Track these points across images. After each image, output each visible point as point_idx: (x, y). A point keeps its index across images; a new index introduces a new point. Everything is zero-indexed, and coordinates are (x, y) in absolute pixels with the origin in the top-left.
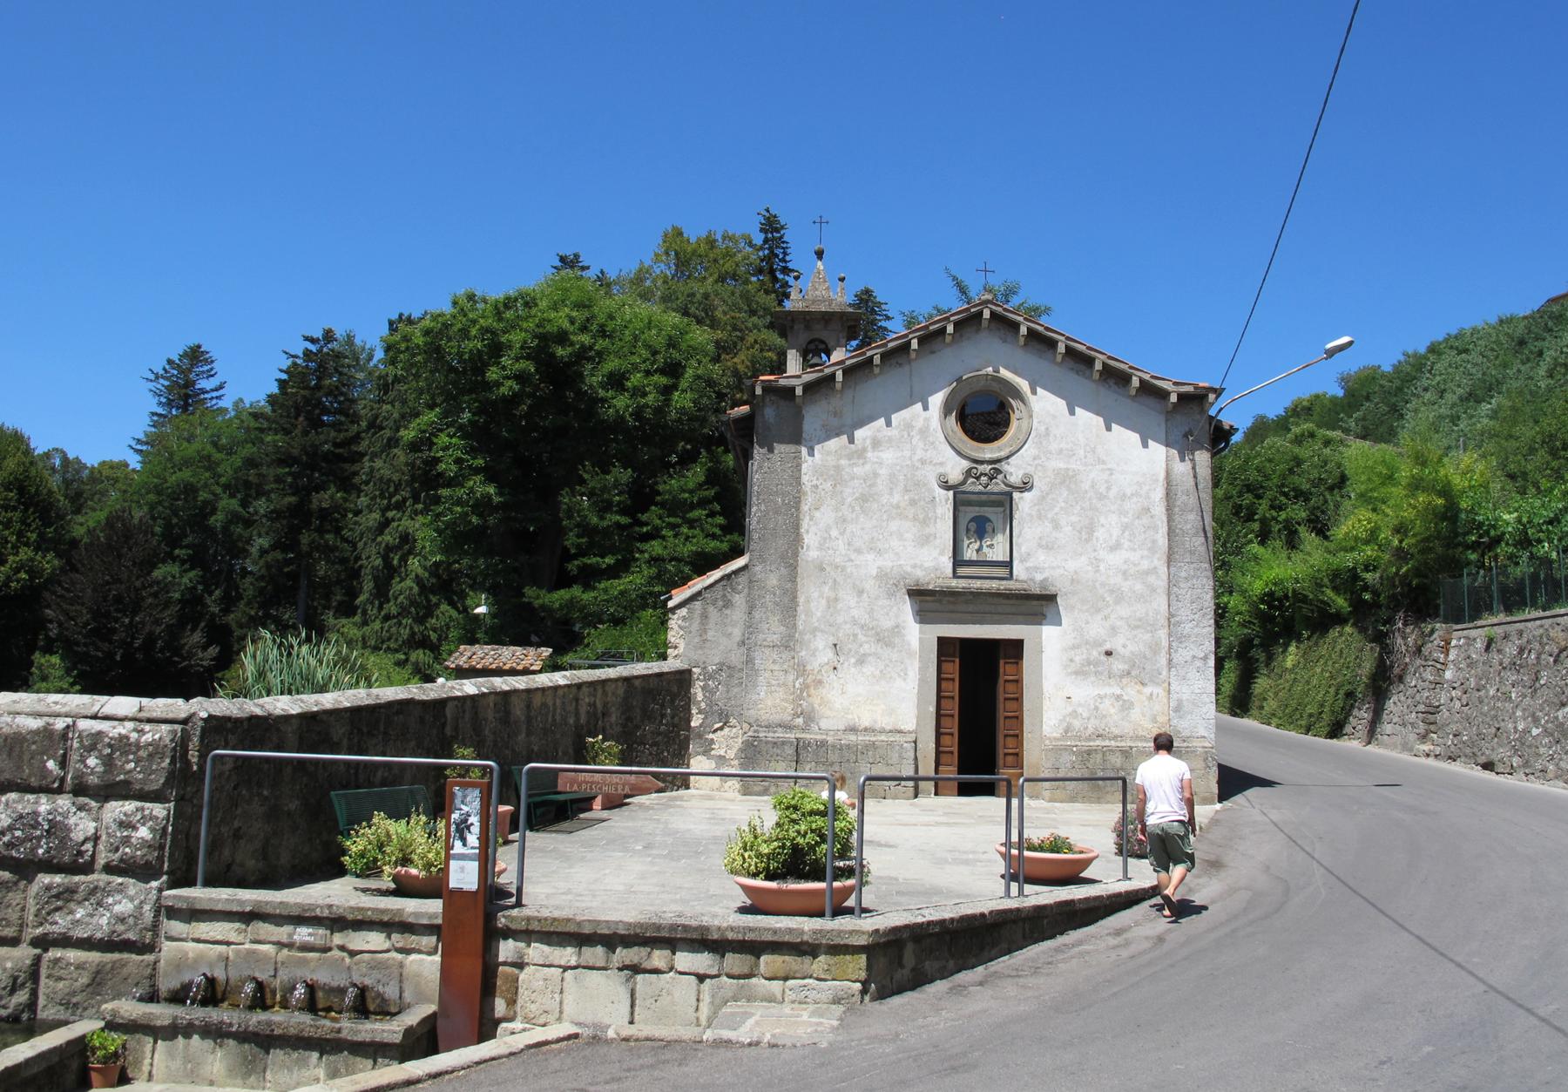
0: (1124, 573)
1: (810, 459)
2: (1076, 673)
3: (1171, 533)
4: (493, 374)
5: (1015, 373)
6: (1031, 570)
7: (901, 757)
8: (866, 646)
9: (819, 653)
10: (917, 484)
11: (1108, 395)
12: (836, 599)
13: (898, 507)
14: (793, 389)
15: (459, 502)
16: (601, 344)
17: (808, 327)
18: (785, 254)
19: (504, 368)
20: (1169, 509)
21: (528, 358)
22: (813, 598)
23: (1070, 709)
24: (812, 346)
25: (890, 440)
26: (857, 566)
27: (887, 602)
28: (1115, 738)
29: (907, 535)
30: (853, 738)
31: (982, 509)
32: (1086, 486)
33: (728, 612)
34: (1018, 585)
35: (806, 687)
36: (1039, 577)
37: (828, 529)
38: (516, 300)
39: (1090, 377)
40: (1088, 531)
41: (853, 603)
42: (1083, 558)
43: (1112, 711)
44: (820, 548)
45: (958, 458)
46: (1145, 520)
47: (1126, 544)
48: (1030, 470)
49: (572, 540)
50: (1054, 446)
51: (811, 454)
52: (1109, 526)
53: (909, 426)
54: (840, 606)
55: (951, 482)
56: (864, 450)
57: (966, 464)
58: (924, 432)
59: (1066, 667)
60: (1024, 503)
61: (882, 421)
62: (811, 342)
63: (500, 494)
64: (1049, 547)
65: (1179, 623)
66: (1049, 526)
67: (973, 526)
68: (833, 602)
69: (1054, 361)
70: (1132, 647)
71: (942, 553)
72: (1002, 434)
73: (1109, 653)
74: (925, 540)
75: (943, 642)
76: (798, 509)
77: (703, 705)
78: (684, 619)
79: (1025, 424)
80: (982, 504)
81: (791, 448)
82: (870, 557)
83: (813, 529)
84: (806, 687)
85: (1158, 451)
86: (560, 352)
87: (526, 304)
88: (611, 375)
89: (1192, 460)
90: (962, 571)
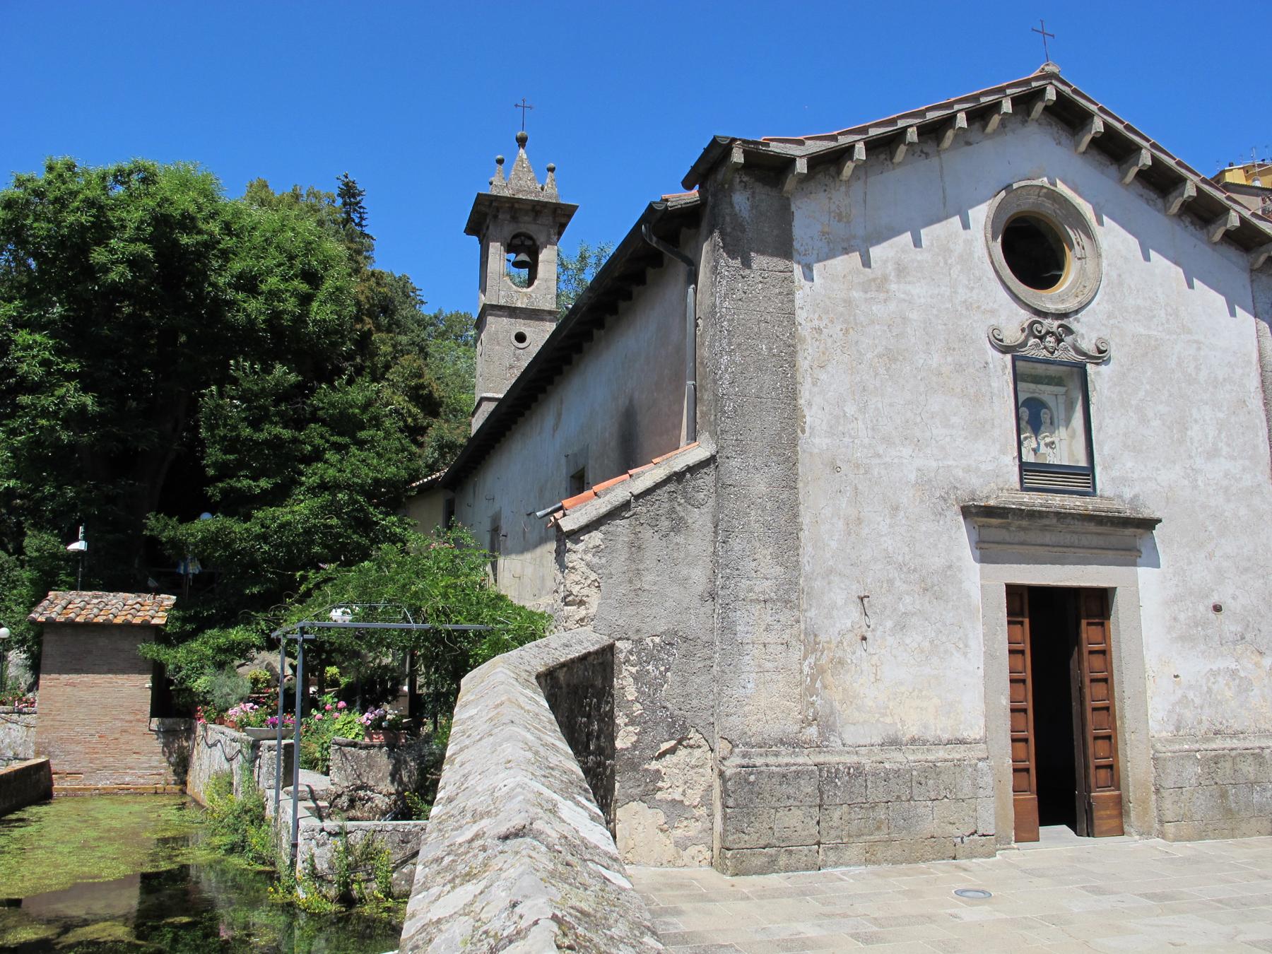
2: (1182, 638)
4: (98, 256)
5: (1075, 190)
6: (1117, 485)
7: (976, 786)
9: (835, 613)
11: (1186, 236)
12: (859, 521)
14: (790, 162)
15: (45, 413)
16: (228, 242)
17: (514, 219)
18: (362, 218)
19: (112, 251)
21: (145, 241)
22: (822, 514)
23: (1179, 693)
24: (517, 242)
28: (1234, 735)
29: (954, 420)
30: (899, 756)
31: (1050, 384)
33: (680, 539)
34: (1104, 505)
35: (819, 671)
36: (1128, 493)
38: (131, 173)
39: (1166, 209)
43: (1228, 694)
45: (1015, 306)
47: (1225, 450)
48: (1105, 333)
49: (214, 454)
54: (865, 531)
55: (1007, 342)
56: (885, 279)
57: (1025, 316)
61: (907, 237)
62: (515, 237)
63: (100, 404)
71: (1003, 451)
73: (1217, 609)
75: (1013, 591)
76: (793, 366)
77: (637, 709)
78: (597, 550)
79: (1090, 265)
81: (780, 263)
82: (906, 451)
83: (818, 400)
84: (819, 671)
85: (1245, 320)
86: (185, 240)
87: (144, 180)
88: (241, 276)
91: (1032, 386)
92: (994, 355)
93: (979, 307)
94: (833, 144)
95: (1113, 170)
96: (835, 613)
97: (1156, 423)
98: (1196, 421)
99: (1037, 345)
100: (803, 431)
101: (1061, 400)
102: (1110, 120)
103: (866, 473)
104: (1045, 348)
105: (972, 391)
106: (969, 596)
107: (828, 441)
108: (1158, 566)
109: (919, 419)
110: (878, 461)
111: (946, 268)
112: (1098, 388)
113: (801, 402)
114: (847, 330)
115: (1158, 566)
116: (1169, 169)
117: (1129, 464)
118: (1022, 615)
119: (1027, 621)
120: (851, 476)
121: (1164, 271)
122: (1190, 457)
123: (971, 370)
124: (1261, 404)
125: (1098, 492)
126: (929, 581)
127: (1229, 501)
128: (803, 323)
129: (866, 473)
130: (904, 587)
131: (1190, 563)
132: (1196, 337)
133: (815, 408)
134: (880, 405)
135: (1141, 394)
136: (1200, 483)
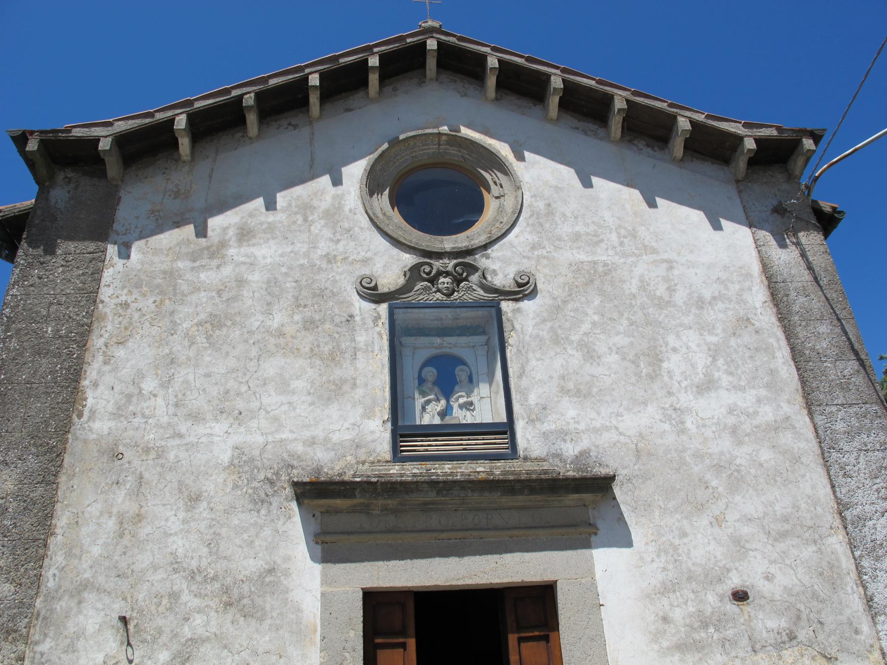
0: (734, 431)
1: (120, 263)
2: (681, 647)
3: (797, 355)
6: (555, 427)
8: (198, 620)
10: (321, 294)
12: (139, 518)
13: (281, 334)
20: (784, 318)
25: (271, 228)
26: (190, 447)
27: (252, 518)
31: (446, 331)
32: (633, 286)
34: (529, 466)
36: (570, 450)
37: (140, 375)
39: (607, 138)
40: (650, 360)
41: (174, 525)
42: (651, 409)
44: (116, 415)
45: (395, 251)
46: (747, 338)
47: (725, 380)
48: (527, 265)
50: (565, 229)
51: (125, 254)
52: (687, 352)
53: (306, 208)
54: (145, 530)
55: (383, 289)
56: (223, 244)
57: (409, 259)
58: (332, 216)
59: (656, 637)
60: (523, 319)
64: (582, 393)
65: (861, 519)
66: (576, 358)
67: (431, 373)
68: (129, 524)
69: (546, 118)
70: (785, 579)
71: (368, 414)
72: (470, 224)
73: (740, 596)
74: (333, 391)
75: (373, 600)
76: (83, 345)
80: (444, 332)
82: (219, 428)
83: (108, 379)
89: (798, 244)
90: (408, 446)
91: (438, 340)
92: (362, 307)
93: (345, 259)
94: (147, 121)
95: (537, 110)
96: (81, 644)
97: (613, 359)
98: (675, 350)
99: (425, 289)
100: (80, 416)
101: (482, 351)
102: (443, 37)
103: (159, 457)
104: (439, 290)
105: (326, 349)
106: (299, 610)
107: (112, 424)
108: (629, 544)
109: (244, 388)
110: (177, 441)
111: (318, 232)
112: (518, 326)
113: (85, 383)
114: (162, 301)
115: (629, 544)
116: (590, 89)
117: (571, 413)
118: (403, 633)
119: (412, 643)
120: (136, 463)
121: (614, 198)
122: (670, 394)
123: (327, 326)
124: (774, 319)
125: (521, 453)
126: (235, 593)
127: (740, 443)
128: (107, 300)
129: (159, 457)
130: (195, 602)
131: (684, 535)
132: (665, 256)
133: (101, 388)
134: (191, 377)
135: (586, 327)
136: (689, 425)
